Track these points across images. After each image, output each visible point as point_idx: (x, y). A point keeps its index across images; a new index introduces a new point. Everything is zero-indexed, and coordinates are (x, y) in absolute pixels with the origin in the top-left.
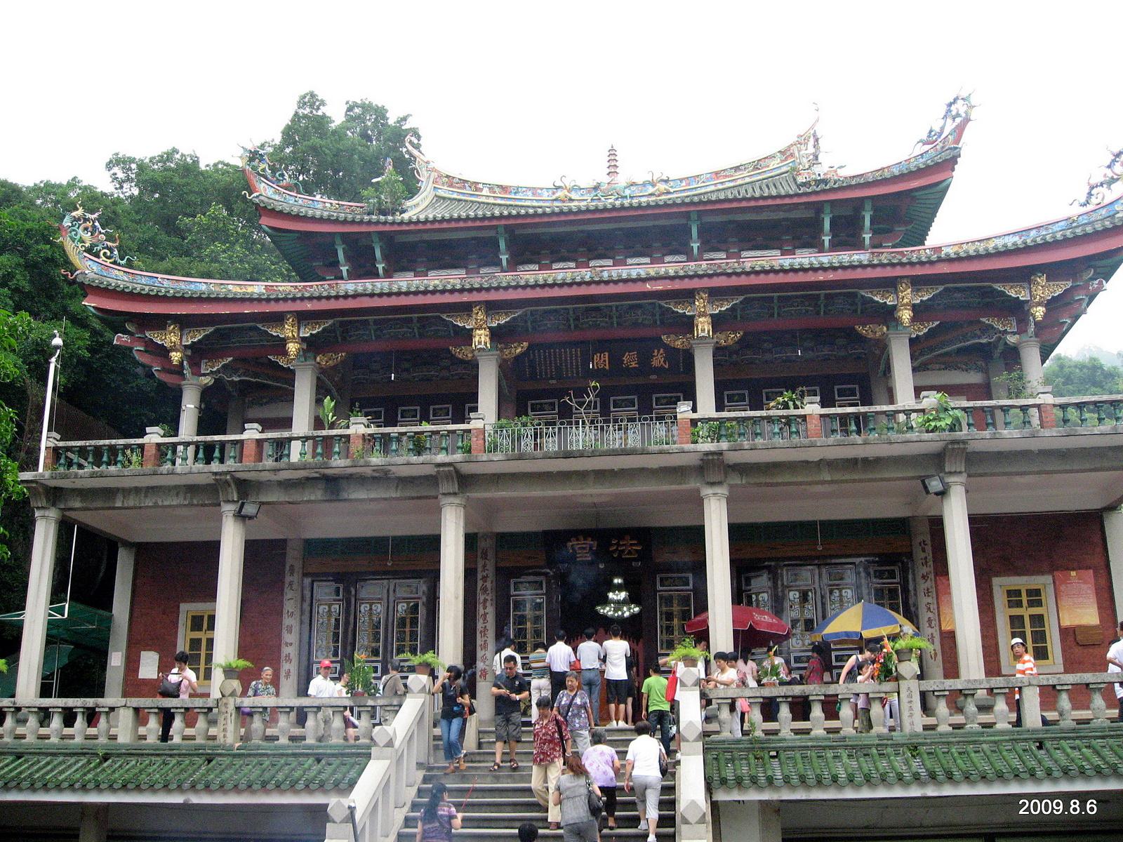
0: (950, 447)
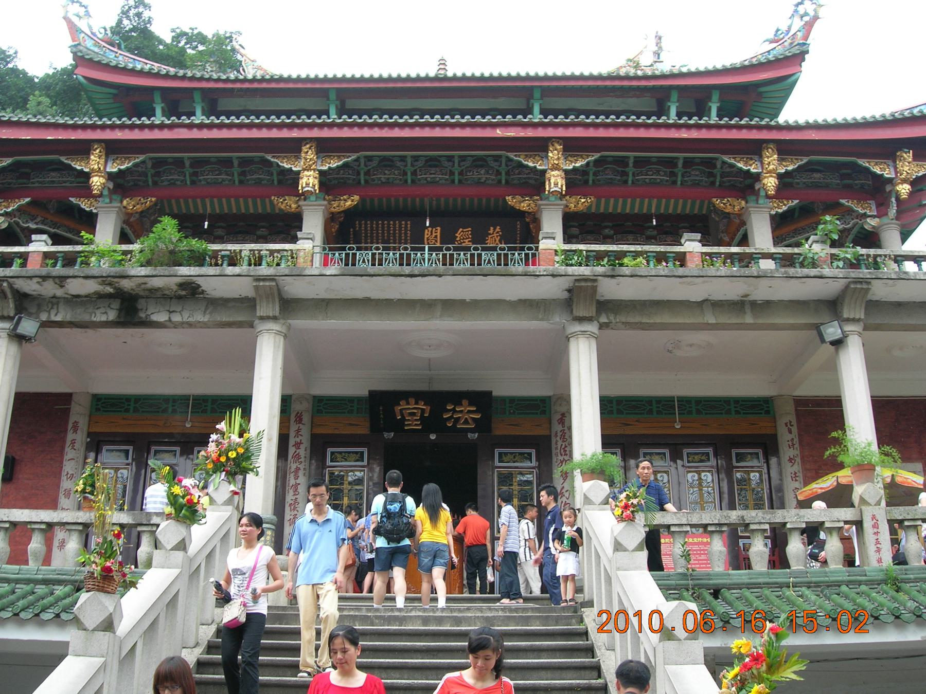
0: (852, 286)
